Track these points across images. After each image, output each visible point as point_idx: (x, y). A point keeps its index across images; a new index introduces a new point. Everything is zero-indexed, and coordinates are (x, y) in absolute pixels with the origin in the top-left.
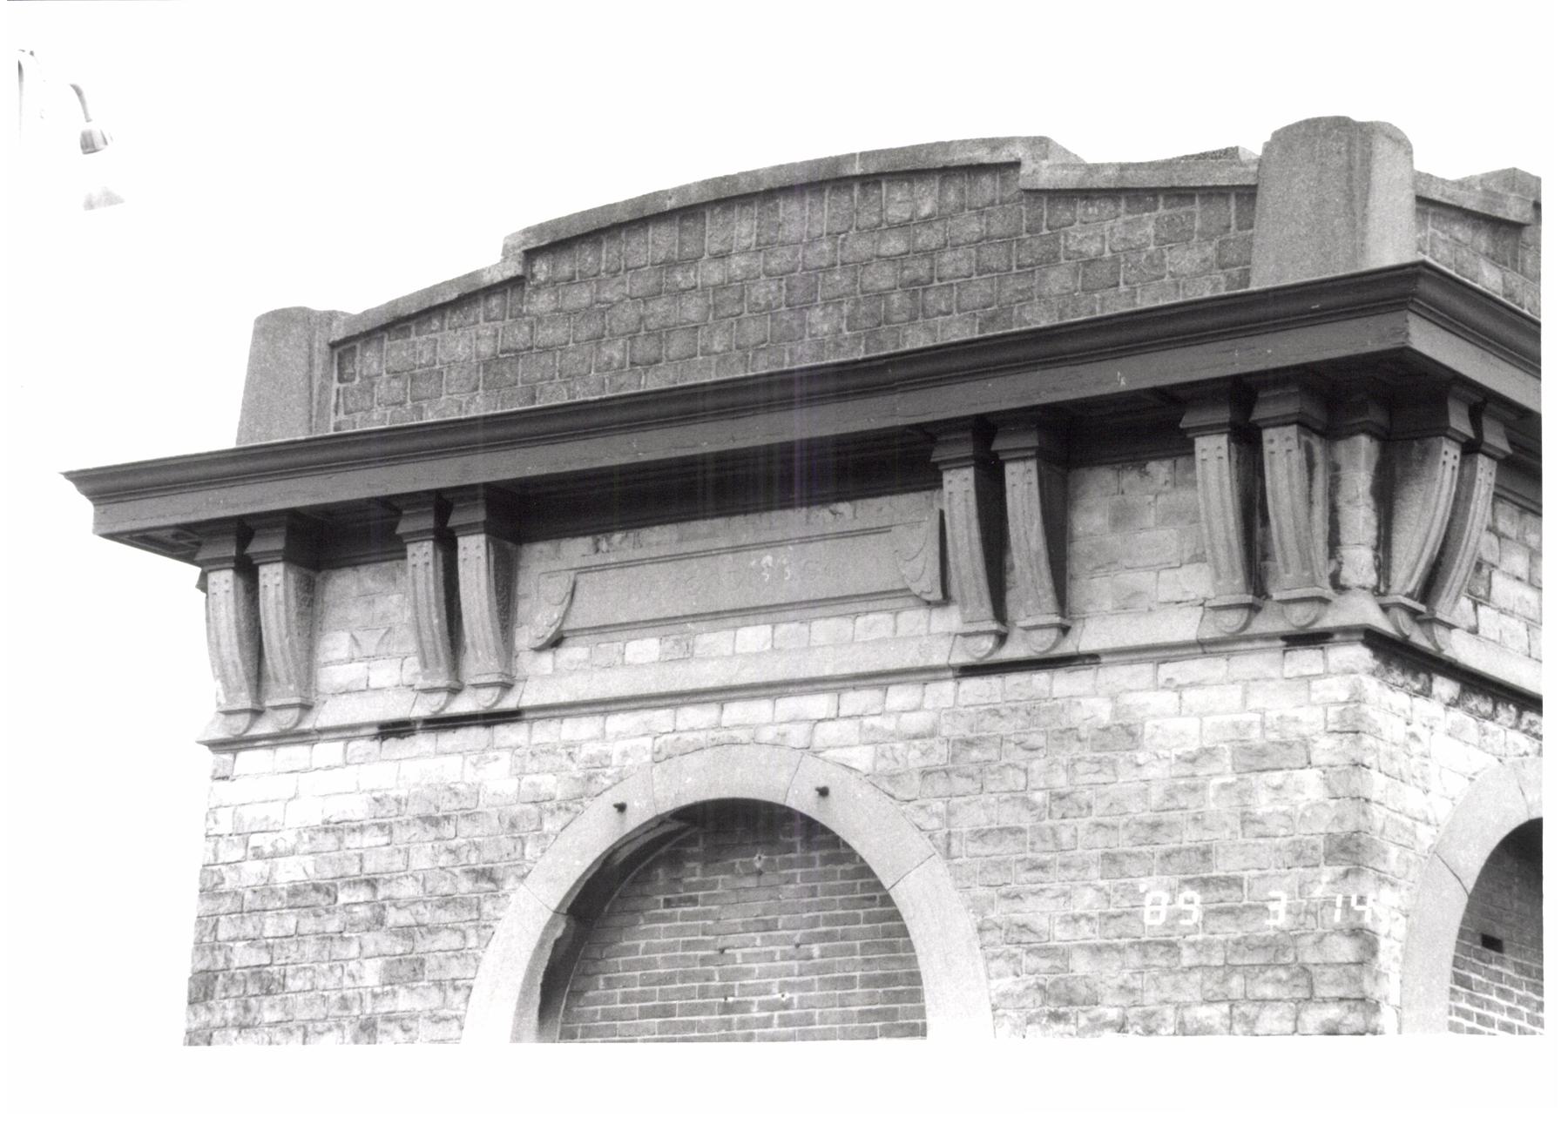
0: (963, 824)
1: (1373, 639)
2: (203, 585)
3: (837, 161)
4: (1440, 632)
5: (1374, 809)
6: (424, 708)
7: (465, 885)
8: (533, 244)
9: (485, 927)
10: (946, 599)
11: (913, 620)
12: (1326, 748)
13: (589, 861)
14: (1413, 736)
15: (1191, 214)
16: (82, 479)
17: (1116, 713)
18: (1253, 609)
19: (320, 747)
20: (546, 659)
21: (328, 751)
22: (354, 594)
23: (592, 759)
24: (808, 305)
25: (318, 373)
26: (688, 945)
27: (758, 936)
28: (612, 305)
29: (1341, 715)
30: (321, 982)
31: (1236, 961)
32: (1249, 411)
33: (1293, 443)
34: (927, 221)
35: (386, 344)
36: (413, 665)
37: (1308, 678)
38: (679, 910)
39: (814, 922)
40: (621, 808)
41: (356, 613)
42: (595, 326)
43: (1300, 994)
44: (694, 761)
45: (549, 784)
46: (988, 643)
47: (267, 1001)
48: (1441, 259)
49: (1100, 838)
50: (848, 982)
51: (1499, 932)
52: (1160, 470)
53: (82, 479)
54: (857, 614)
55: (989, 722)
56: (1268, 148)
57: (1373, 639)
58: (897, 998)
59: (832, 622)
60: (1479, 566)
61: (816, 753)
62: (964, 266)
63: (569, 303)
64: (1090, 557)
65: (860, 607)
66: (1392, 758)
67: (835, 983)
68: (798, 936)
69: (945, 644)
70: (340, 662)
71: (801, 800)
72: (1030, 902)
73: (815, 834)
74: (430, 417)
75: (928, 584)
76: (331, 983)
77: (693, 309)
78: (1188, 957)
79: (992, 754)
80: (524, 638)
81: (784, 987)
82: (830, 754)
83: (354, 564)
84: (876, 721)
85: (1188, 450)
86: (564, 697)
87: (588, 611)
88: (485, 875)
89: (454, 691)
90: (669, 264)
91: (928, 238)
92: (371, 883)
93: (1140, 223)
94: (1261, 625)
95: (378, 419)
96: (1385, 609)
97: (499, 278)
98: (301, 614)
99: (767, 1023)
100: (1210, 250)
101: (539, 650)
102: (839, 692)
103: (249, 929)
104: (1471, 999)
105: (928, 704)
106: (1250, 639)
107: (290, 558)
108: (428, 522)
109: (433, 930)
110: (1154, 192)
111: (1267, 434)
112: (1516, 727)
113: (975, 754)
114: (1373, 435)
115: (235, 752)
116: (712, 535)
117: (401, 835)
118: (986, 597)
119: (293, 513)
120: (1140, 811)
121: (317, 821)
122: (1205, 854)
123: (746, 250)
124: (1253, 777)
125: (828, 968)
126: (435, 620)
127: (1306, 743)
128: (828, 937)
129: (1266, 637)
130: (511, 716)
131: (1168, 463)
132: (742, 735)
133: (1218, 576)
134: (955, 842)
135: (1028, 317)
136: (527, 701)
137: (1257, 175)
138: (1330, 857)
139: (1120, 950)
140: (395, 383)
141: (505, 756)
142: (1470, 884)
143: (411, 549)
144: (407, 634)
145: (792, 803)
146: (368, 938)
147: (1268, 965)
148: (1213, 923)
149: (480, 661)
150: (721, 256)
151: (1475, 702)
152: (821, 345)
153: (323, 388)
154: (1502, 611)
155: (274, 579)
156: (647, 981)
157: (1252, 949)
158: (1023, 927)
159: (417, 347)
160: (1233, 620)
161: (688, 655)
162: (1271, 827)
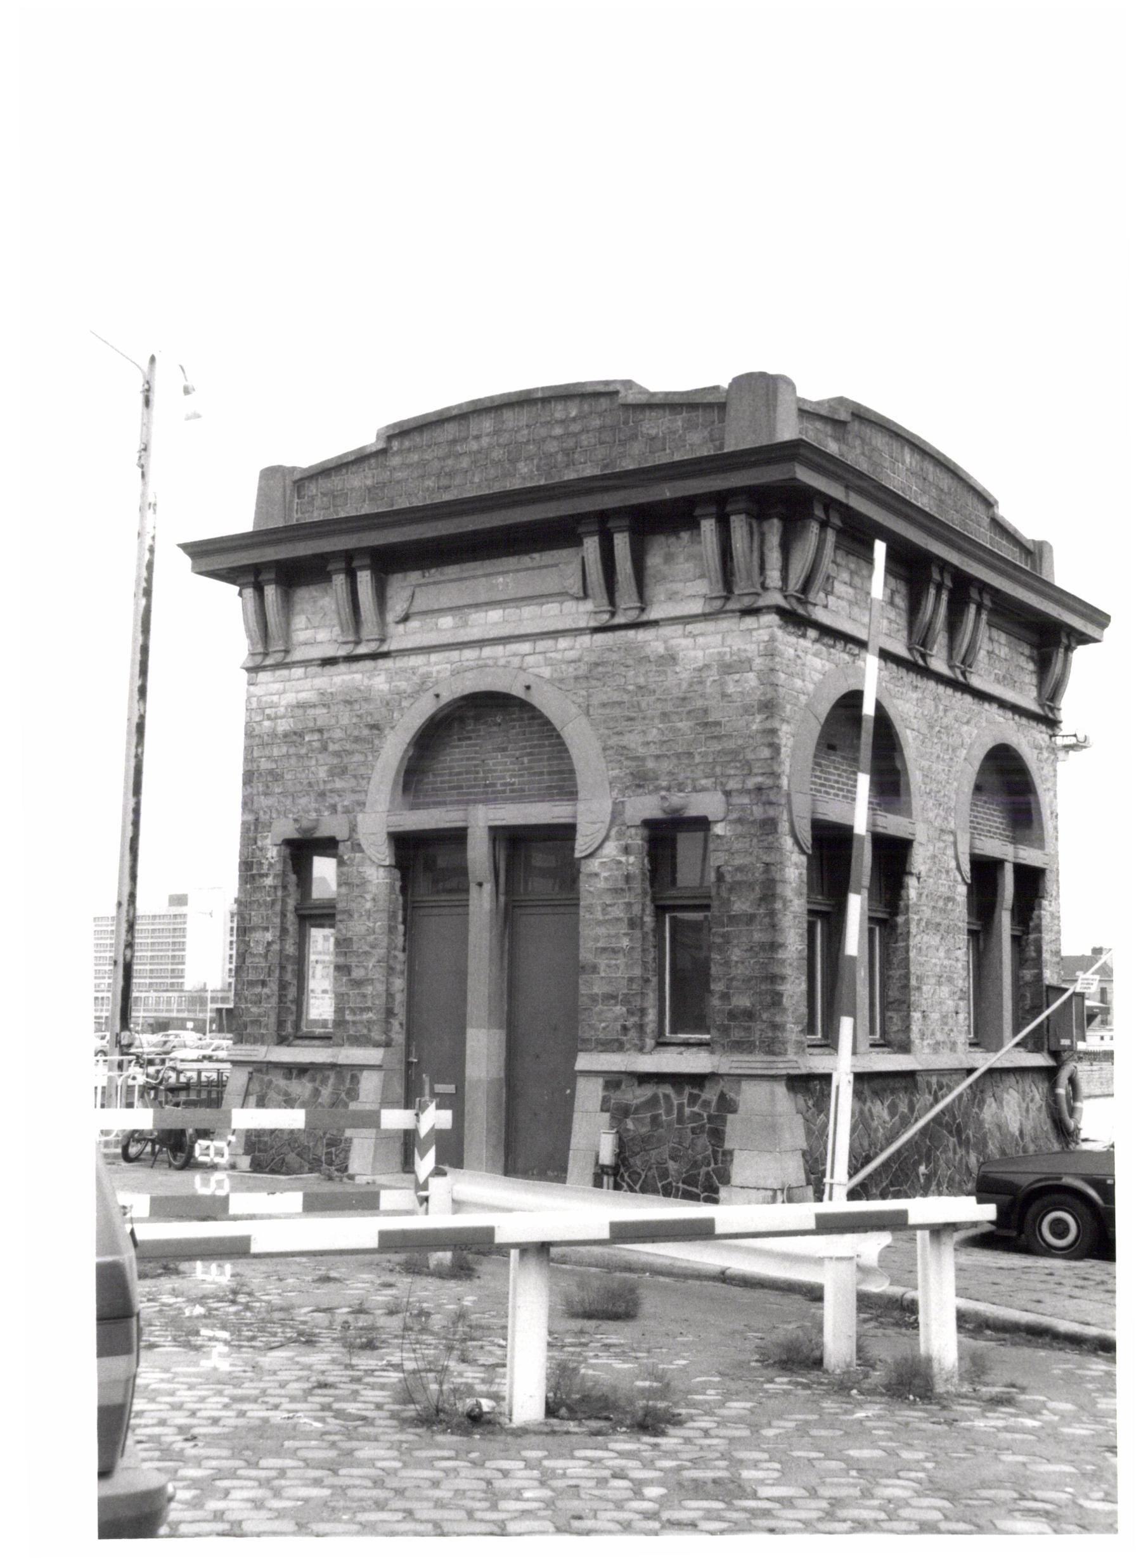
0: (595, 701)
1: (780, 611)
2: (240, 594)
3: (529, 392)
4: (810, 608)
5: (780, 689)
6: (342, 652)
7: (366, 732)
8: (391, 432)
9: (375, 751)
10: (586, 596)
11: (570, 606)
12: (758, 663)
13: (423, 720)
14: (798, 656)
15: (697, 416)
16: (185, 547)
17: (666, 649)
18: (727, 599)
19: (293, 670)
20: (401, 627)
21: (298, 672)
22: (593, 1033)
23: (423, 675)
24: (518, 460)
25: (288, 492)
26: (468, 759)
27: (499, 755)
28: (429, 461)
29: (766, 647)
30: (298, 775)
31: (719, 760)
32: (724, 507)
33: (744, 524)
34: (574, 419)
35: (320, 481)
36: (337, 630)
37: (750, 631)
38: (464, 743)
39: (525, 748)
40: (437, 696)
41: (308, 607)
42: (420, 471)
43: (745, 772)
44: (469, 675)
45: (403, 685)
46: (606, 617)
47: (276, 784)
48: (810, 438)
49: (659, 705)
50: (542, 773)
51: (835, 742)
52: (685, 536)
53: (185, 547)
54: (543, 604)
55: (607, 654)
56: (731, 385)
57: (780, 611)
58: (564, 780)
59: (532, 608)
60: (828, 578)
61: (525, 670)
62: (593, 441)
63: (408, 461)
64: (655, 577)
65: (544, 600)
66: (788, 666)
67: (534, 774)
68: (518, 753)
69: (586, 617)
70: (302, 629)
71: (517, 691)
72: (627, 736)
73: (524, 706)
74: (342, 515)
75: (577, 588)
76: (304, 776)
77: (465, 463)
78: (698, 759)
79: (609, 669)
80: (391, 617)
81: (512, 776)
82: (531, 670)
83: (308, 585)
84: (552, 655)
85: (697, 526)
86: (410, 646)
87: (420, 604)
88: (375, 727)
89: (357, 643)
90: (454, 442)
91: (575, 428)
92: (320, 731)
93: (676, 420)
94: (731, 606)
95: (317, 516)
96: (786, 597)
97: (374, 449)
98: (283, 607)
99: (504, 792)
100: (706, 434)
101: (398, 623)
102: (535, 641)
103: (267, 753)
104: (821, 771)
105: (577, 646)
106: (726, 612)
107: (278, 582)
108: (343, 565)
109: (351, 753)
110: (681, 405)
111: (733, 518)
112: (844, 651)
113: (600, 669)
114: (781, 519)
115: (257, 673)
116: (474, 569)
117: (334, 709)
118: (606, 596)
119: (277, 562)
120: (676, 693)
121: (294, 702)
122: (706, 711)
123: (488, 435)
124: (726, 677)
125: (531, 768)
126: (347, 611)
127: (750, 661)
128: (531, 754)
129: (733, 611)
130: (386, 655)
131: (689, 533)
132: (490, 662)
133: (711, 584)
134: (591, 709)
135: (624, 464)
136: (393, 647)
137: (726, 398)
138: (760, 711)
139: (668, 757)
140: (325, 499)
141: (383, 673)
142: (822, 720)
143: (334, 577)
144: (334, 616)
145: (514, 693)
146: (320, 756)
147: (732, 761)
148: (709, 743)
149: (369, 628)
150: (477, 438)
151: (826, 640)
152: (524, 479)
153: (291, 502)
154: (839, 598)
155: (270, 591)
156: (450, 774)
157: (726, 754)
158: (624, 747)
159: (336, 482)
160: (718, 604)
161: (465, 625)
162: (734, 698)
